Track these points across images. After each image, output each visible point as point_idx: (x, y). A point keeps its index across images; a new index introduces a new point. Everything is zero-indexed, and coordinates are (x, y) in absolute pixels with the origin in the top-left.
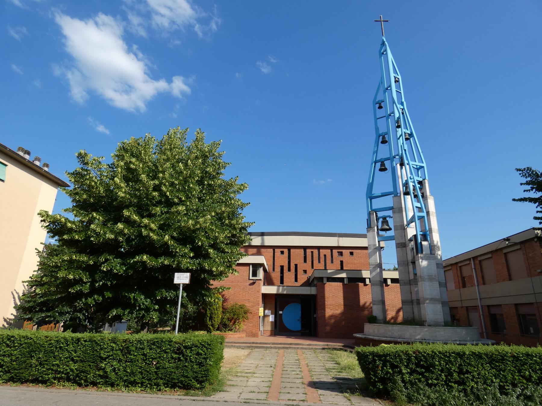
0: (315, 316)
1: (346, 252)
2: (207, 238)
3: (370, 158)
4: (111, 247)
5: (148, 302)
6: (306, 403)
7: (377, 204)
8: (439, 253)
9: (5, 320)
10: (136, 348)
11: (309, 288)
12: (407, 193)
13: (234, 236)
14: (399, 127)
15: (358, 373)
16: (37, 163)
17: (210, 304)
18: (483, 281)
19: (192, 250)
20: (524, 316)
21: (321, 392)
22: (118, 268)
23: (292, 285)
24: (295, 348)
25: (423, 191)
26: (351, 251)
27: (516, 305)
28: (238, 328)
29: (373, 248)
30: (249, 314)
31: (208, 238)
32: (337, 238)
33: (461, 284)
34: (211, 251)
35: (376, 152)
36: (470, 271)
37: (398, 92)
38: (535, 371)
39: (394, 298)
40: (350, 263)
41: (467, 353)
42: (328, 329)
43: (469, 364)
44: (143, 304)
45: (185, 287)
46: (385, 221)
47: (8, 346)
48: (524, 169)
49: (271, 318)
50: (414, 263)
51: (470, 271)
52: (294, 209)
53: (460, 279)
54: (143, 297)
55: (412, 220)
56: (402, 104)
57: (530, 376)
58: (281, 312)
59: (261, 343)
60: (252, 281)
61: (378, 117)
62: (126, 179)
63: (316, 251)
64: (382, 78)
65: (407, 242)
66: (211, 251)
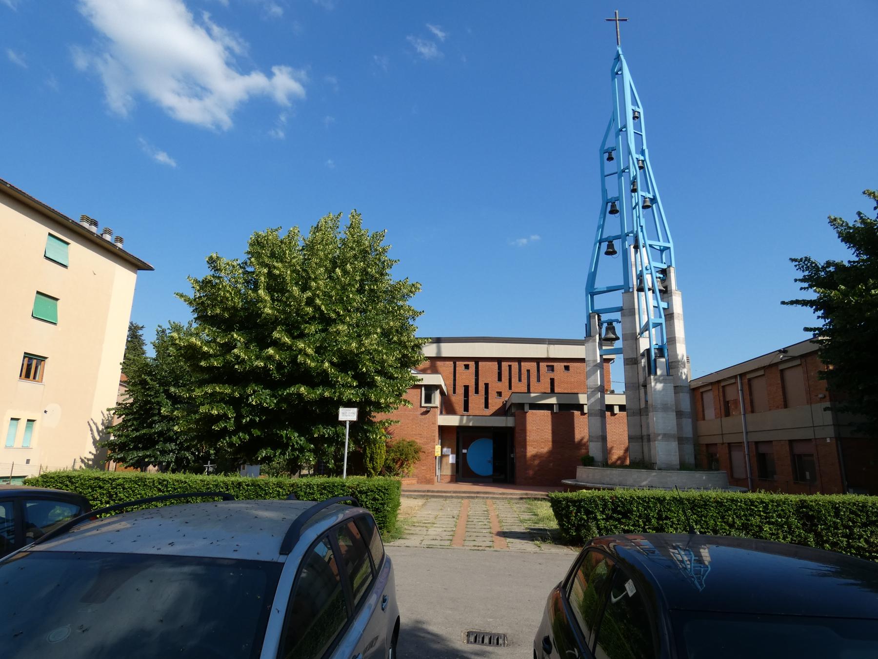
0: (512, 456)
1: (559, 366)
2: (373, 363)
3: (592, 235)
4: (261, 377)
5: (302, 441)
6: (492, 549)
7: (600, 302)
8: (685, 371)
9: (82, 461)
10: (305, 493)
11: (504, 418)
12: (641, 289)
13: (404, 356)
14: (634, 190)
15: (554, 525)
16: (108, 237)
17: (375, 441)
18: (752, 408)
19: (354, 377)
20: (800, 456)
21: (509, 540)
22: (268, 401)
23: (480, 413)
24: (483, 498)
25: (666, 283)
26: (566, 364)
27: (791, 442)
28: (406, 471)
29: (592, 364)
30: (421, 454)
31: (372, 360)
32: (545, 346)
33: (723, 411)
34: (378, 378)
35: (602, 227)
36: (735, 393)
37: (638, 135)
38: (739, 517)
39: (618, 433)
40: (565, 382)
41: (668, 498)
42: (531, 472)
43: (669, 510)
44: (297, 443)
45: (352, 423)
46: (611, 328)
47: (159, 490)
48: (801, 259)
49: (452, 459)
50: (645, 386)
51: (735, 393)
52: (483, 305)
53: (722, 403)
54: (296, 435)
55: (646, 328)
56: (643, 153)
57: (734, 522)
58: (465, 451)
59: (438, 492)
60: (425, 409)
61: (606, 173)
62: (269, 289)
63: (515, 365)
64: (614, 113)
65: (640, 358)
66: (378, 378)
